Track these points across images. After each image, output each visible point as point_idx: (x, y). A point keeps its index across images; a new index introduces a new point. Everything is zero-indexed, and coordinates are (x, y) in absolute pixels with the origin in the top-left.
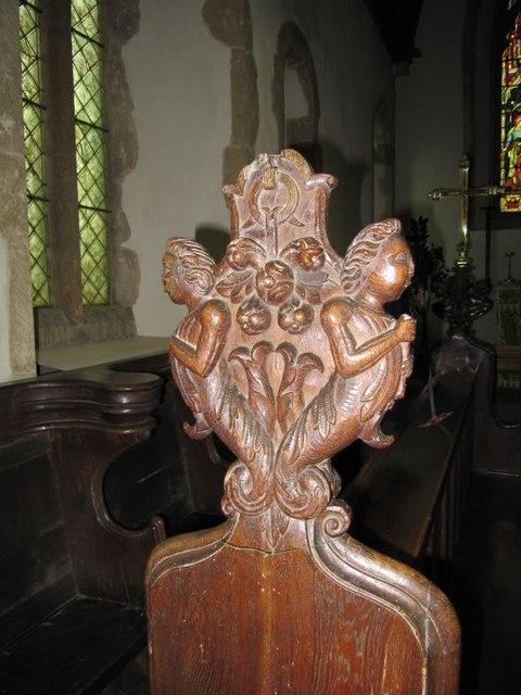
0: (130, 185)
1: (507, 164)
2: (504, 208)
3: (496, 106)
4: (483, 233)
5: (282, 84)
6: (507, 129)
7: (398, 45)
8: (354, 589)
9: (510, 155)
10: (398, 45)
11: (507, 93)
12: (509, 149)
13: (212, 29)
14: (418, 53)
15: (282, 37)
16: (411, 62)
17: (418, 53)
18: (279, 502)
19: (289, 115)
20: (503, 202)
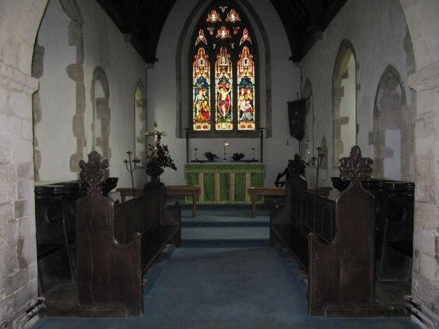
0: (37, 127)
1: (196, 110)
2: (195, 129)
3: (191, 86)
4: (185, 139)
5: (94, 91)
6: (196, 95)
7: (148, 55)
8: (332, 225)
9: (197, 106)
10: (148, 55)
11: (195, 81)
12: (197, 103)
13: (69, 75)
14: (157, 60)
15: (94, 73)
16: (154, 63)
17: (157, 60)
18: (206, 161)
19: (96, 97)
20: (195, 126)
